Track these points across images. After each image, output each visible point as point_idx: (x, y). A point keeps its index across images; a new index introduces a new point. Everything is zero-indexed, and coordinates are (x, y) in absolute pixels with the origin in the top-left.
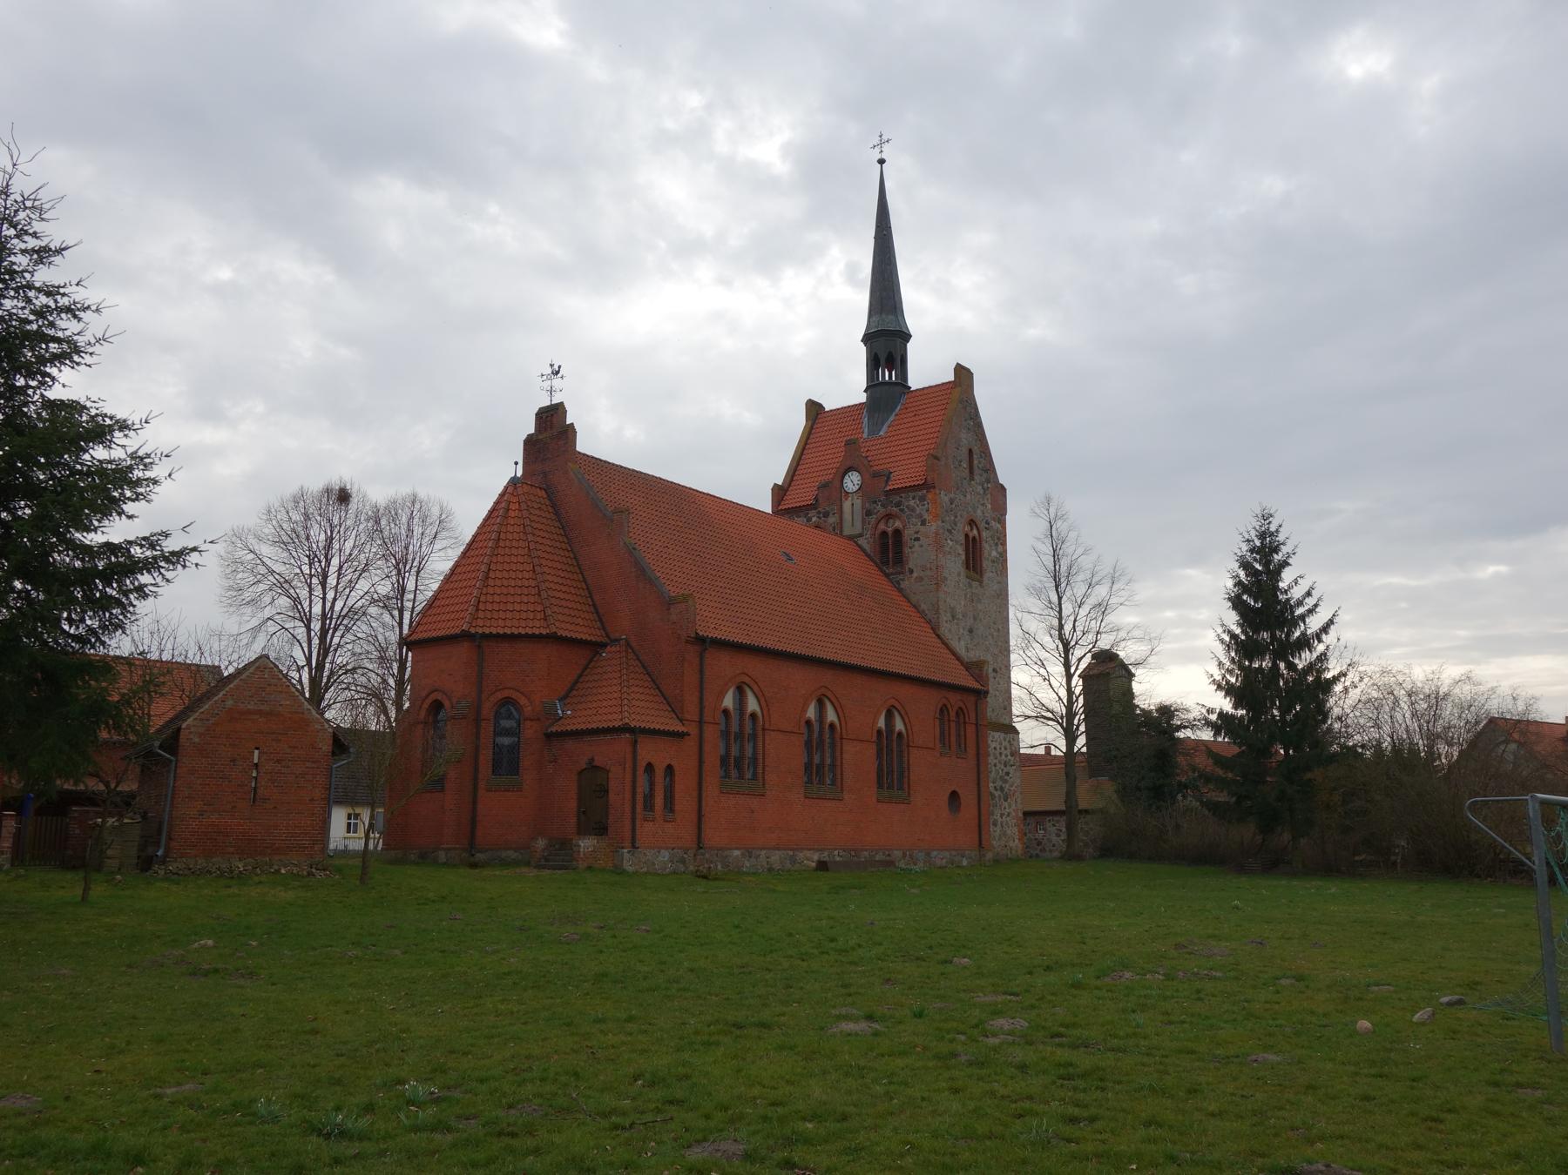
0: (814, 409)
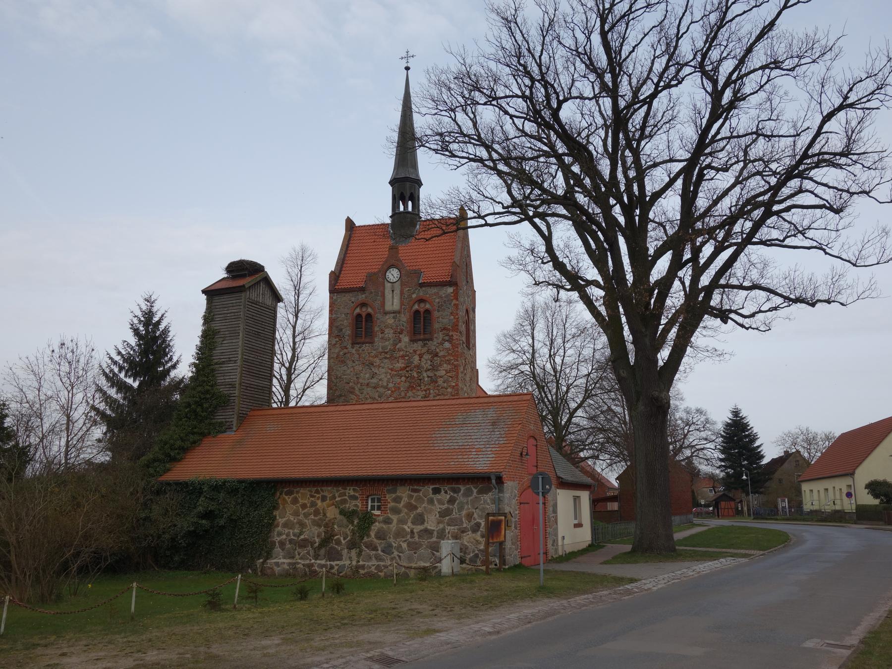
0: (350, 224)
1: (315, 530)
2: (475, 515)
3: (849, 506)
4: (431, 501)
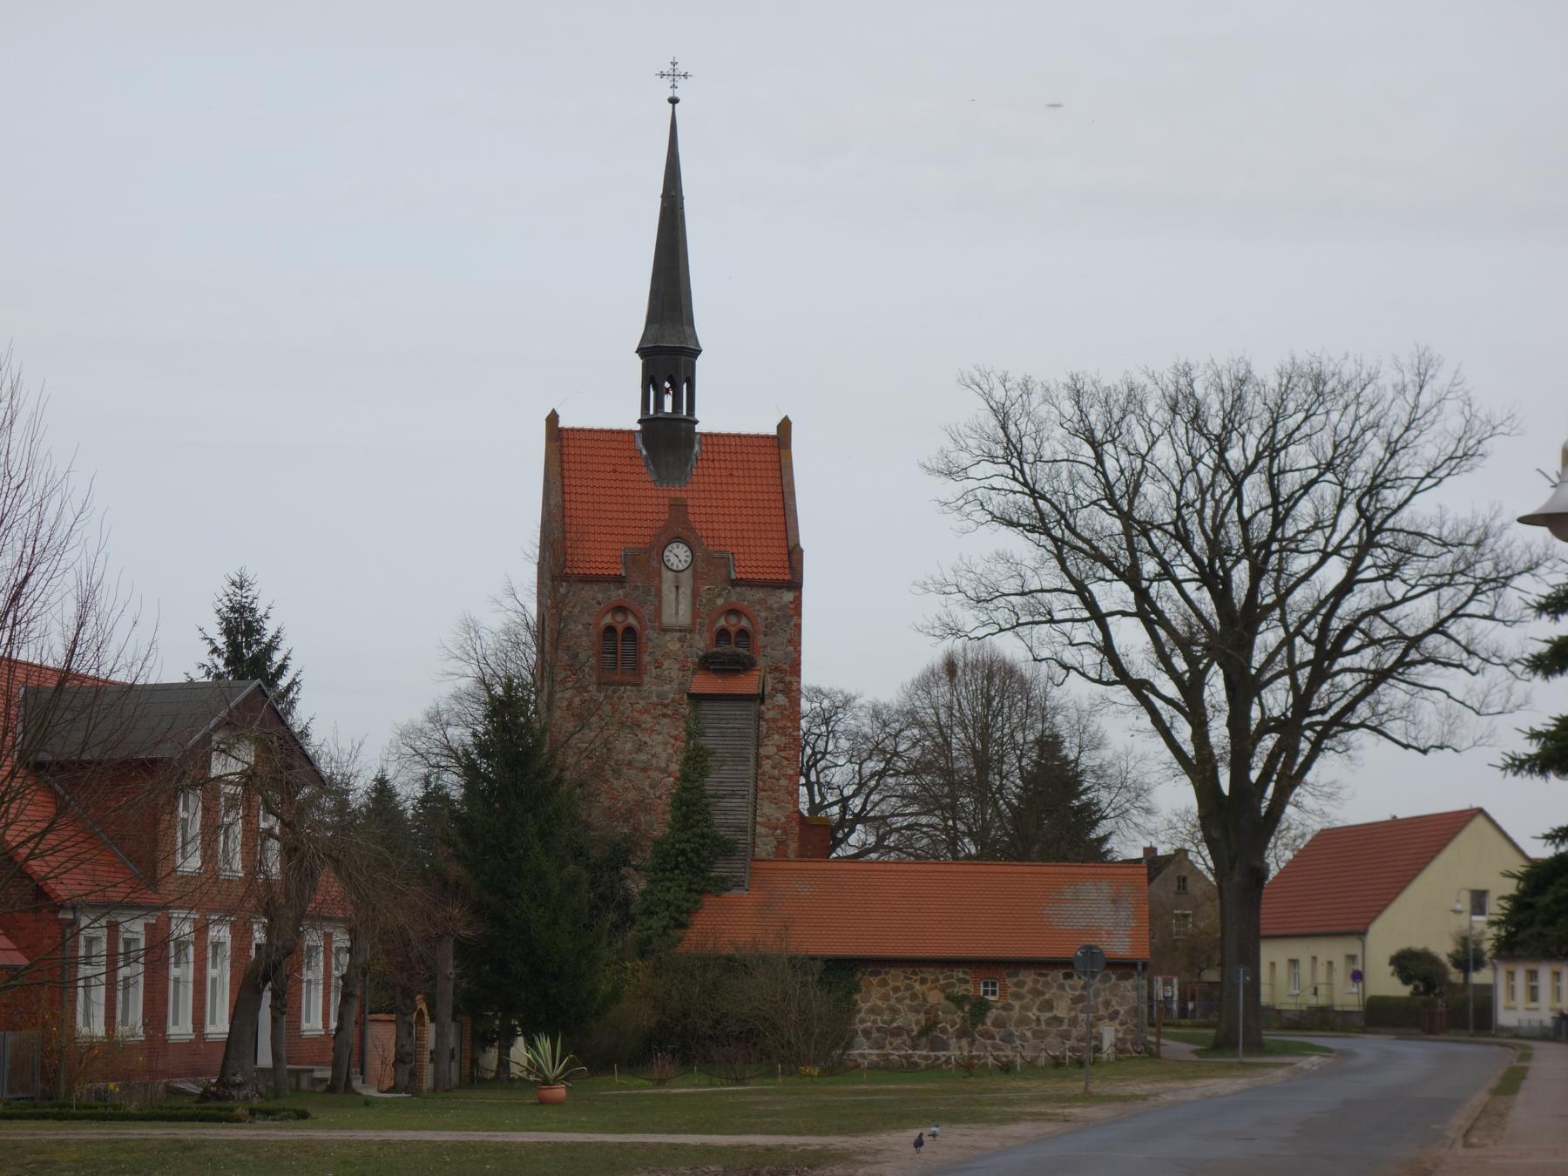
1: (912, 1017)
2: (1114, 1003)
3: (1347, 997)
4: (1061, 987)
